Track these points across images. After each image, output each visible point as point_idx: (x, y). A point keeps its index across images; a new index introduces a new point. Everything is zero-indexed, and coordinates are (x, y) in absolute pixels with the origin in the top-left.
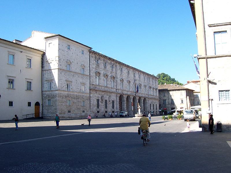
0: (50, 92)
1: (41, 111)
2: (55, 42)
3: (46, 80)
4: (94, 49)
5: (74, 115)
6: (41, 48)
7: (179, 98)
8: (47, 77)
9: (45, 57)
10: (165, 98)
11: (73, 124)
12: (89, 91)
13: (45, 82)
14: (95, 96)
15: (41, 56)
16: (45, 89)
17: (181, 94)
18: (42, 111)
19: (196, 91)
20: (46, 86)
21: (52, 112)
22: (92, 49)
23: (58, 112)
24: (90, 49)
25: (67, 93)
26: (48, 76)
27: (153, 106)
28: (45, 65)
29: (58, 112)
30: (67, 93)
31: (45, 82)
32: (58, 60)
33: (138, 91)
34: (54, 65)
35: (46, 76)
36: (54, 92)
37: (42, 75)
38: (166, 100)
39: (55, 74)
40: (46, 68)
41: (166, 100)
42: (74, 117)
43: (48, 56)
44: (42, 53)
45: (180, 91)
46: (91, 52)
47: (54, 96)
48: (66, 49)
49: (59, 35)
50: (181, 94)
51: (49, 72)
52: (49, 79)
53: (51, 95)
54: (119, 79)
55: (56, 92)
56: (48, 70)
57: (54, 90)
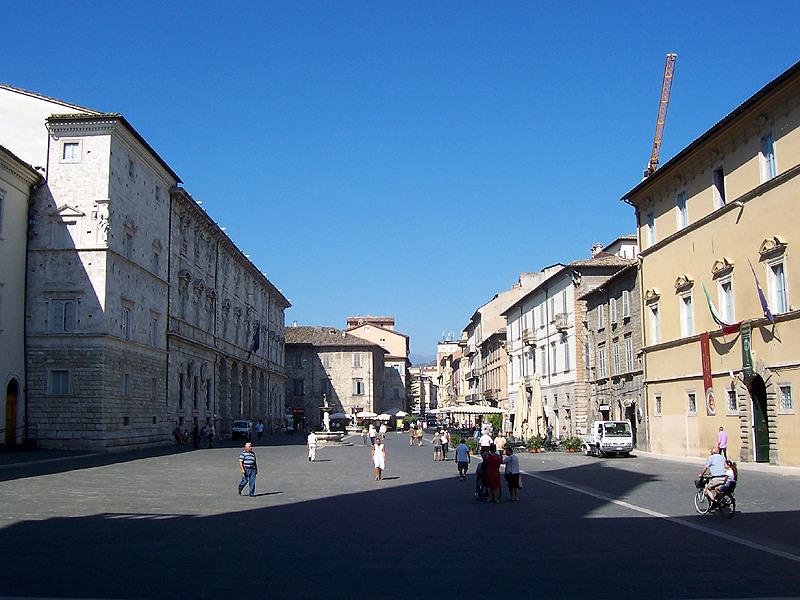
0: (67, 342)
1: (21, 422)
2: (98, 149)
3: (45, 292)
4: (186, 186)
5: (137, 434)
6: (34, 159)
7: (348, 376)
8: (49, 276)
9: (45, 195)
10: (301, 374)
11: (629, 466)
12: (165, 343)
13: (41, 300)
14: (177, 360)
15: (25, 188)
16: (37, 327)
17: (357, 365)
18: (26, 418)
19: (393, 354)
20: (46, 316)
21: (74, 421)
22: (179, 185)
23: (102, 421)
24: (173, 182)
25: (121, 346)
26: (55, 275)
27: (195, 402)
28: (42, 227)
29: (102, 421)
30: (121, 346)
31: (41, 300)
32: (106, 214)
33: (256, 347)
34: (89, 236)
35: (45, 274)
36: (85, 341)
37: (28, 269)
38: (302, 381)
39: (96, 270)
40: (45, 240)
41: (302, 381)
42: (137, 440)
43: (61, 192)
44: (32, 178)
45: (353, 354)
46: (180, 197)
47: (85, 359)
48: (125, 177)
49: (122, 120)
50: (357, 365)
51: (60, 259)
52: (60, 288)
53: (71, 353)
54: (221, 300)
55: (97, 342)
56: (57, 250)
57: (85, 332)
